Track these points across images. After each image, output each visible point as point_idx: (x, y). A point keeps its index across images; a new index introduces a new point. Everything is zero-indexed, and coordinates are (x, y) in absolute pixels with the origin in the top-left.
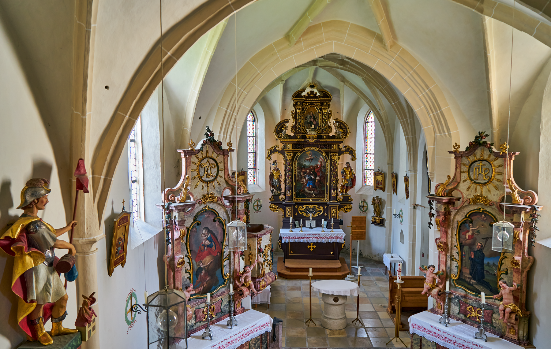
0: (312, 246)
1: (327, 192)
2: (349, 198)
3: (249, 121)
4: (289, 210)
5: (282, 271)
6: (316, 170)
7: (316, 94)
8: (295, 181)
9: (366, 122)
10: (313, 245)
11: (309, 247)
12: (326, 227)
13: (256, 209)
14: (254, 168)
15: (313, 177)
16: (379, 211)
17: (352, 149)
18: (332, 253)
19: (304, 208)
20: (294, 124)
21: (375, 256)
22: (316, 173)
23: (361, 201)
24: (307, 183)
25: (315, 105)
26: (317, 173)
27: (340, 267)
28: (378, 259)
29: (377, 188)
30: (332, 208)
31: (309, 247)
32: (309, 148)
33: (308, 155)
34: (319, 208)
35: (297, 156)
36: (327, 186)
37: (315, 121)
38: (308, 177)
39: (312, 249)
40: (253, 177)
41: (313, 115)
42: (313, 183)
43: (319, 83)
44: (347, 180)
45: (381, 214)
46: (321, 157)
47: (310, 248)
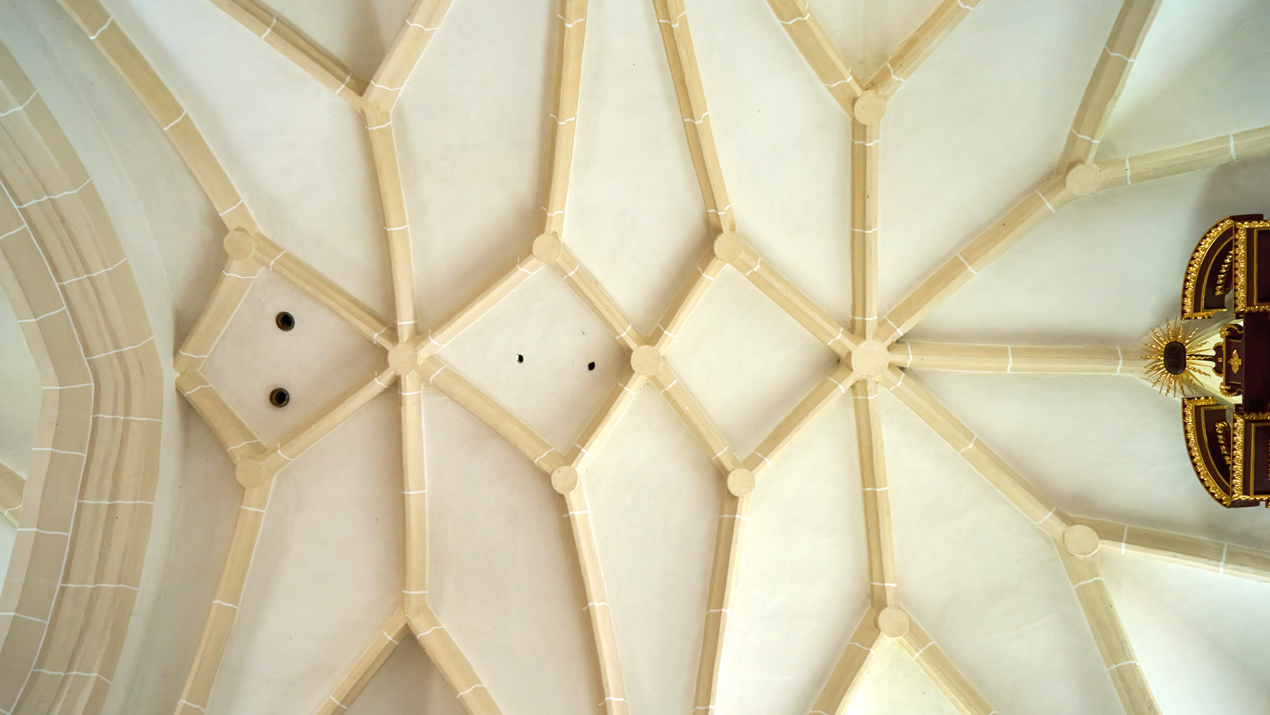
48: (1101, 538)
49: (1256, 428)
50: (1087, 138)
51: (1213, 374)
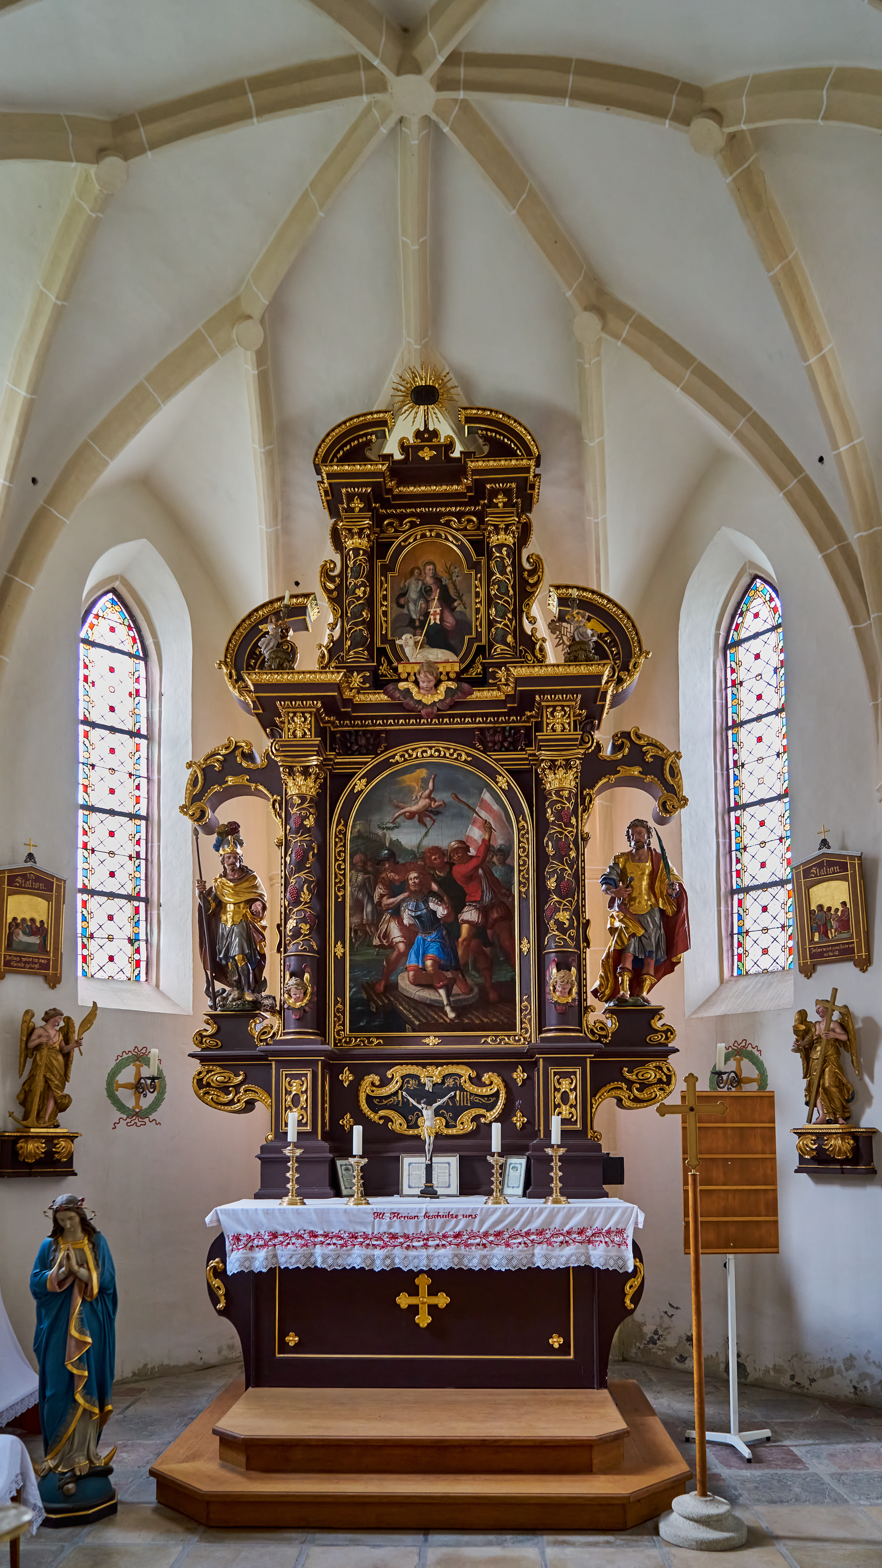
0: (424, 1300)
1: (525, 991)
2: (657, 1024)
3: (429, 1169)
4: (294, 1090)
5: (187, 1466)
6: (460, 871)
7: (450, 446)
8: (340, 937)
9: (727, 647)
10: (432, 1292)
11: (404, 1300)
12: (520, 1191)
13: (130, 1103)
14: (138, 898)
15: (441, 911)
16: (841, 1085)
17: (661, 748)
18: (556, 1341)
19: (393, 1087)
20: (337, 633)
21: (829, 1372)
22: (461, 888)
23: (721, 1046)
24: (409, 945)
25: (447, 524)
26: (469, 888)
27: (617, 1437)
28: (848, 1391)
29: (821, 955)
30: (552, 1071)
31: (404, 1300)
32: (423, 751)
33: (411, 790)
34: (477, 1081)
35: (353, 796)
36: (523, 957)
37: (453, 610)
38: (417, 908)
39: (423, 1320)
40: (131, 941)
41: (437, 579)
42: (443, 947)
43: (467, 384)
44: (639, 920)
45: (853, 1107)
46: (487, 796)
47: (414, 1310)
48: (256, 352)
49: (380, 482)
50: (624, 335)
51: (414, 429)
